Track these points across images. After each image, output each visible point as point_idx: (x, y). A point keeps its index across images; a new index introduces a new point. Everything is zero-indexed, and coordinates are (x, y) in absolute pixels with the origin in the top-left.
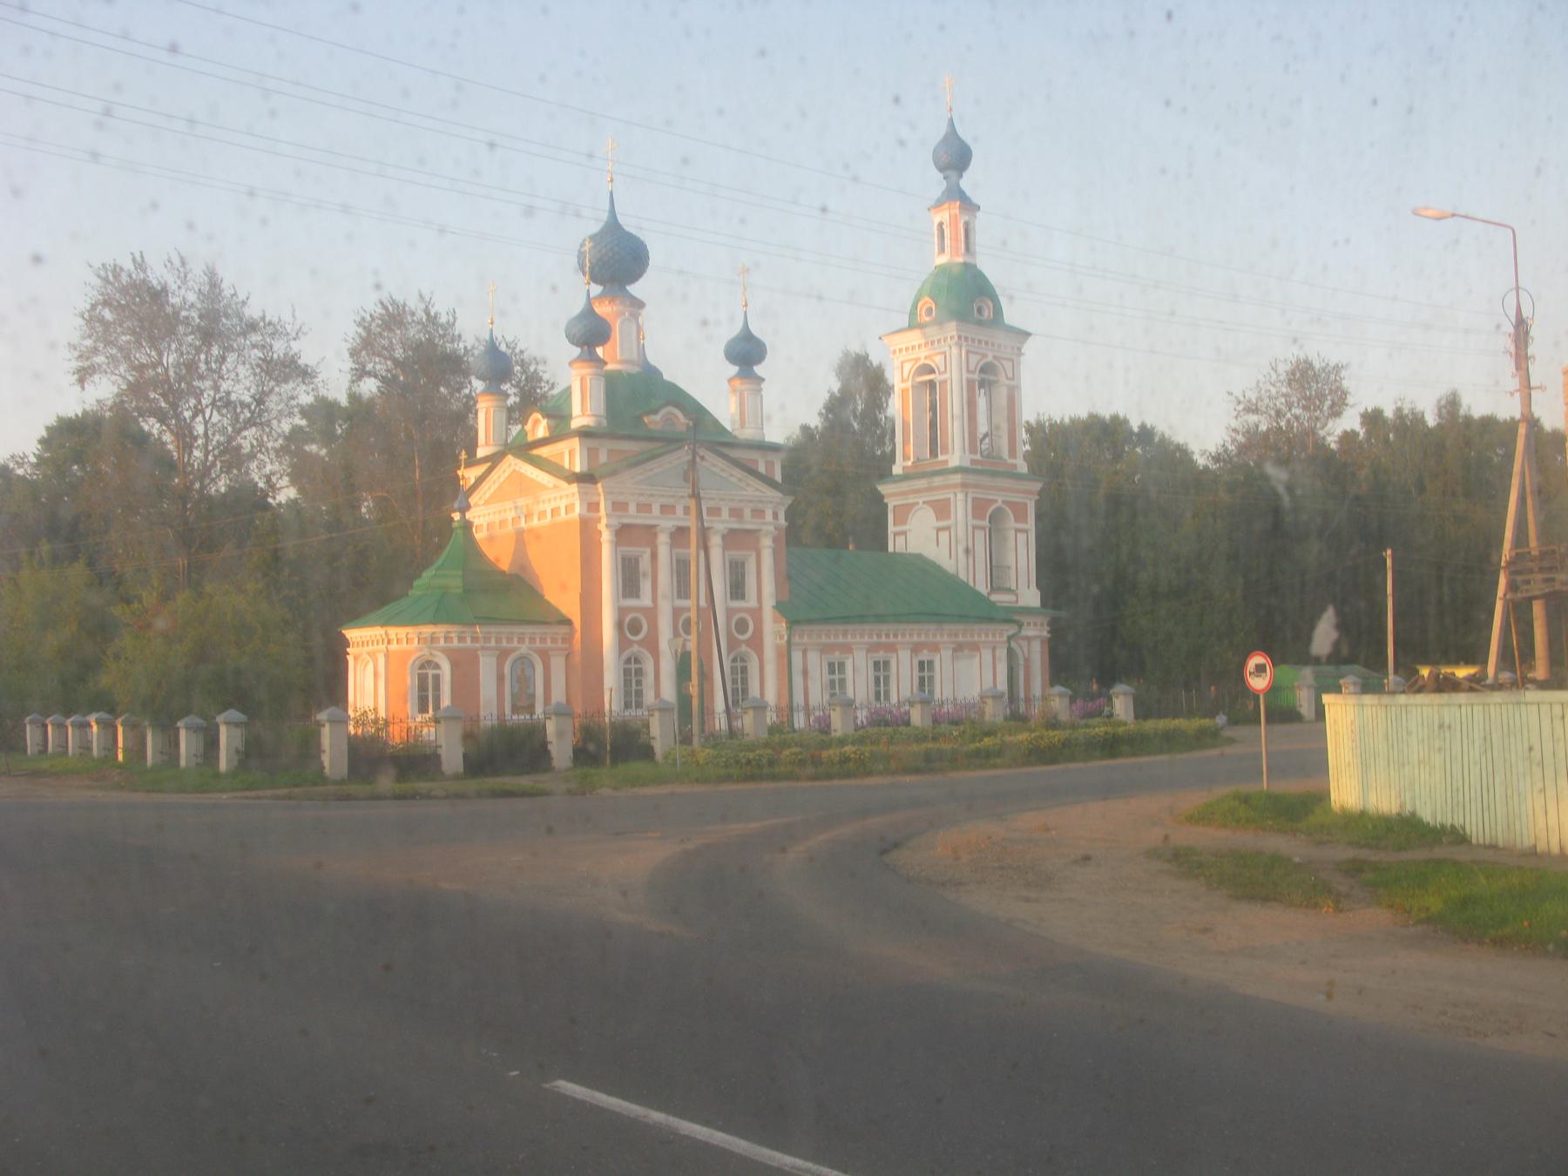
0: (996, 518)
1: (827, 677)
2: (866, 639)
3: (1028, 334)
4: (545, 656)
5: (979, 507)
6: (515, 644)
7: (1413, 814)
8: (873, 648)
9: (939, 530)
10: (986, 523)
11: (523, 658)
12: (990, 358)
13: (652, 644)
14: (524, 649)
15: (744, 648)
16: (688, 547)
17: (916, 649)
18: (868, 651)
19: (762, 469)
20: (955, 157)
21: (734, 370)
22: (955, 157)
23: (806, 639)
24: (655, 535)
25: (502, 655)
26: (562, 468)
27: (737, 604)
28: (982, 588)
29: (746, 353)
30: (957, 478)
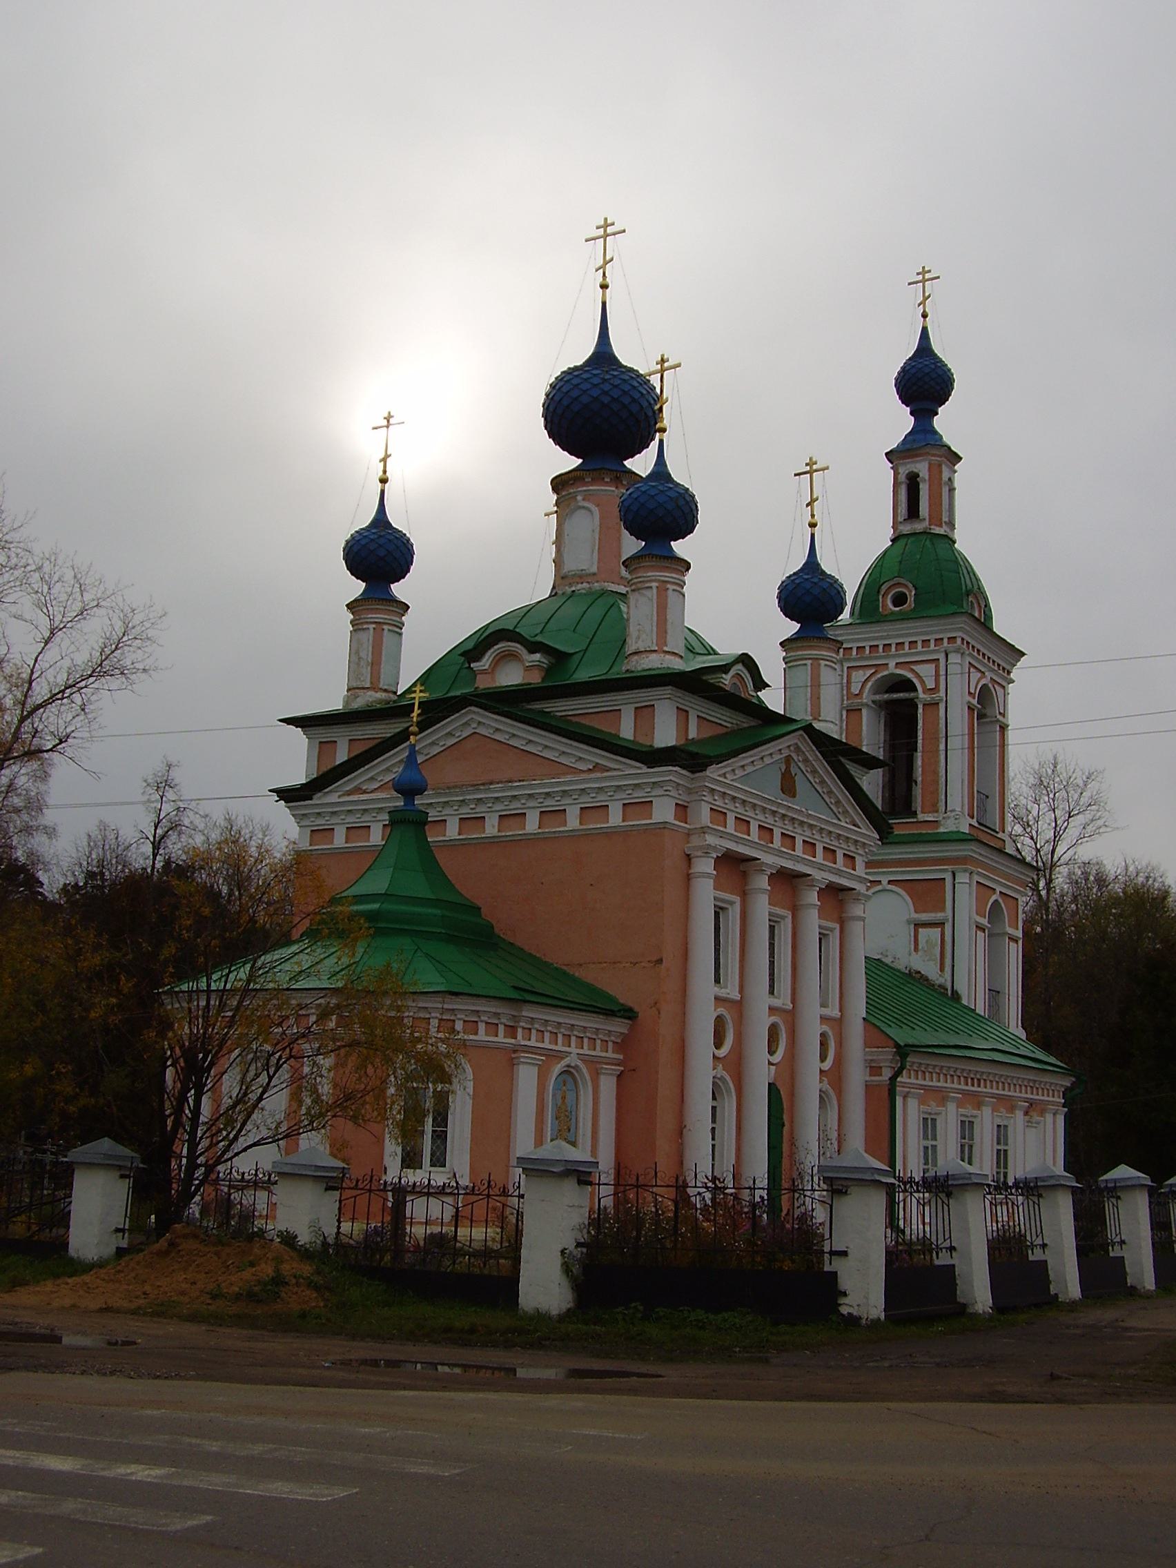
3: (1023, 654)
9: (918, 925)
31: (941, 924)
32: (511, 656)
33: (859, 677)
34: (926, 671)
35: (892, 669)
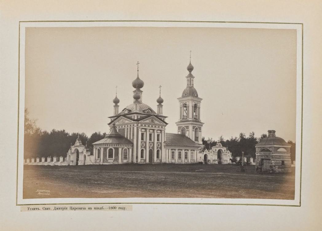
0: (196, 129)
1: (181, 156)
2: (178, 148)
4: (129, 149)
5: (194, 127)
6: (109, 146)
7: (74, 133)
8: (191, 150)
10: (194, 130)
11: (126, 149)
12: (196, 103)
13: (145, 147)
14: (126, 148)
15: (159, 149)
16: (112, 158)
17: (172, 150)
18: (178, 150)
19: (162, 119)
20: (190, 69)
21: (158, 104)
22: (190, 69)
23: (169, 148)
24: (146, 130)
25: (122, 149)
26: (132, 118)
27: (150, 141)
28: (193, 140)
29: (160, 101)
30: (191, 122)
31: (188, 131)
32: (126, 110)
33: (181, 104)
34: (188, 103)
35: (184, 103)
